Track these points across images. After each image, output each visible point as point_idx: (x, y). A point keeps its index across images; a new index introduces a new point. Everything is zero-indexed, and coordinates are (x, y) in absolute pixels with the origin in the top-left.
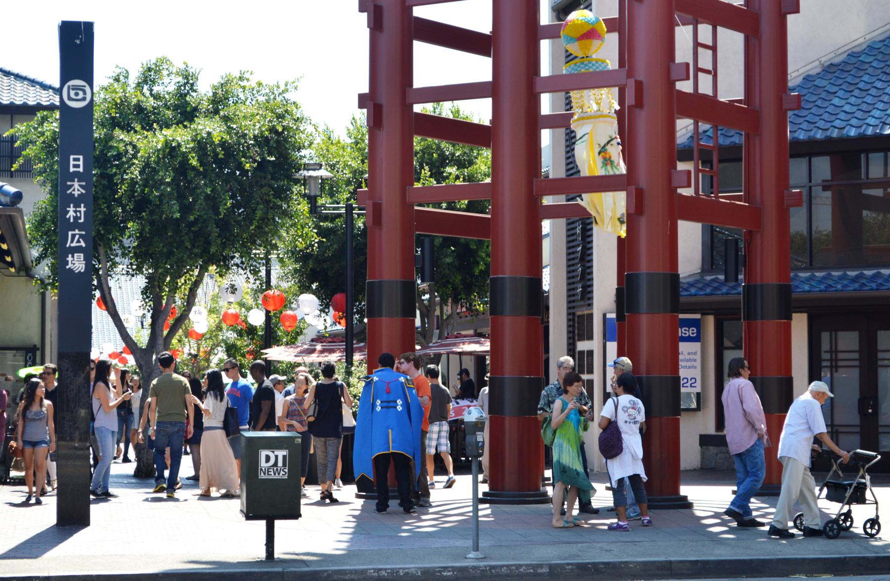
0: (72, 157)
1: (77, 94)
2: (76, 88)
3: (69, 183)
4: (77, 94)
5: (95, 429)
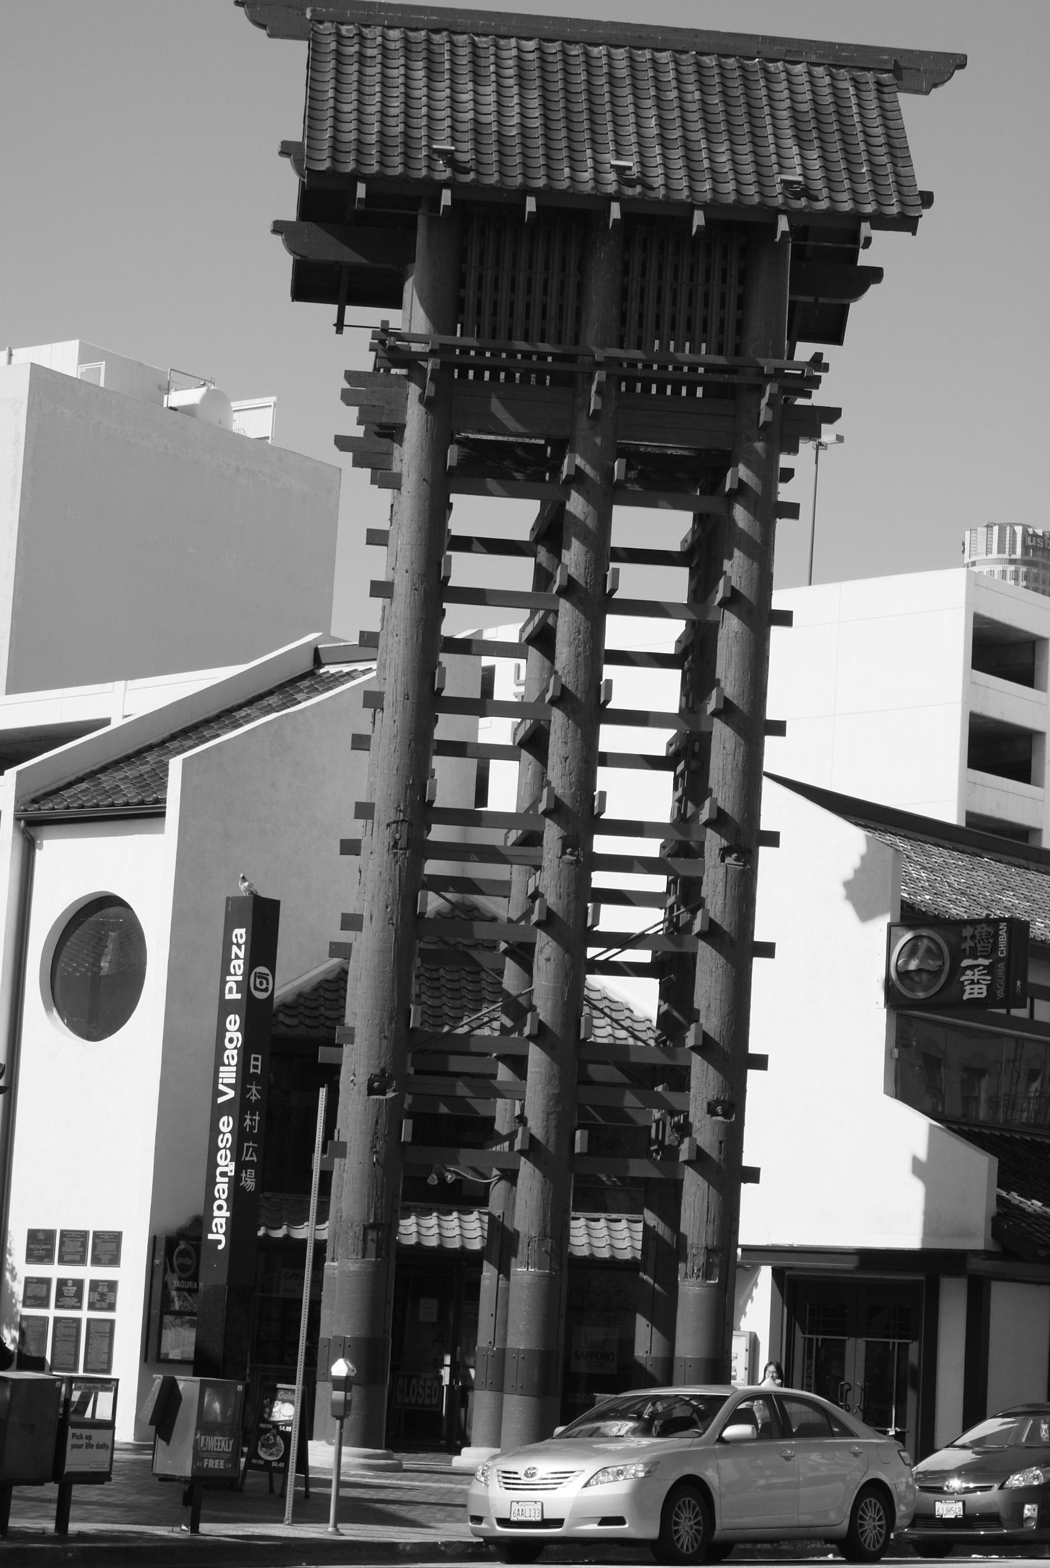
0: (253, 1056)
1: (261, 983)
2: (262, 976)
3: (248, 1086)
4: (261, 983)
5: (677, 1365)
